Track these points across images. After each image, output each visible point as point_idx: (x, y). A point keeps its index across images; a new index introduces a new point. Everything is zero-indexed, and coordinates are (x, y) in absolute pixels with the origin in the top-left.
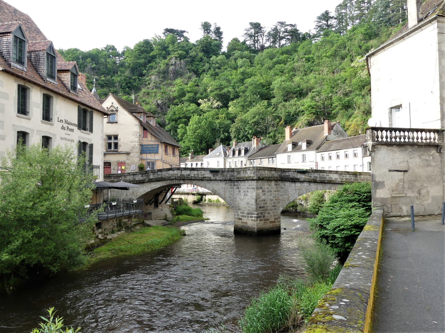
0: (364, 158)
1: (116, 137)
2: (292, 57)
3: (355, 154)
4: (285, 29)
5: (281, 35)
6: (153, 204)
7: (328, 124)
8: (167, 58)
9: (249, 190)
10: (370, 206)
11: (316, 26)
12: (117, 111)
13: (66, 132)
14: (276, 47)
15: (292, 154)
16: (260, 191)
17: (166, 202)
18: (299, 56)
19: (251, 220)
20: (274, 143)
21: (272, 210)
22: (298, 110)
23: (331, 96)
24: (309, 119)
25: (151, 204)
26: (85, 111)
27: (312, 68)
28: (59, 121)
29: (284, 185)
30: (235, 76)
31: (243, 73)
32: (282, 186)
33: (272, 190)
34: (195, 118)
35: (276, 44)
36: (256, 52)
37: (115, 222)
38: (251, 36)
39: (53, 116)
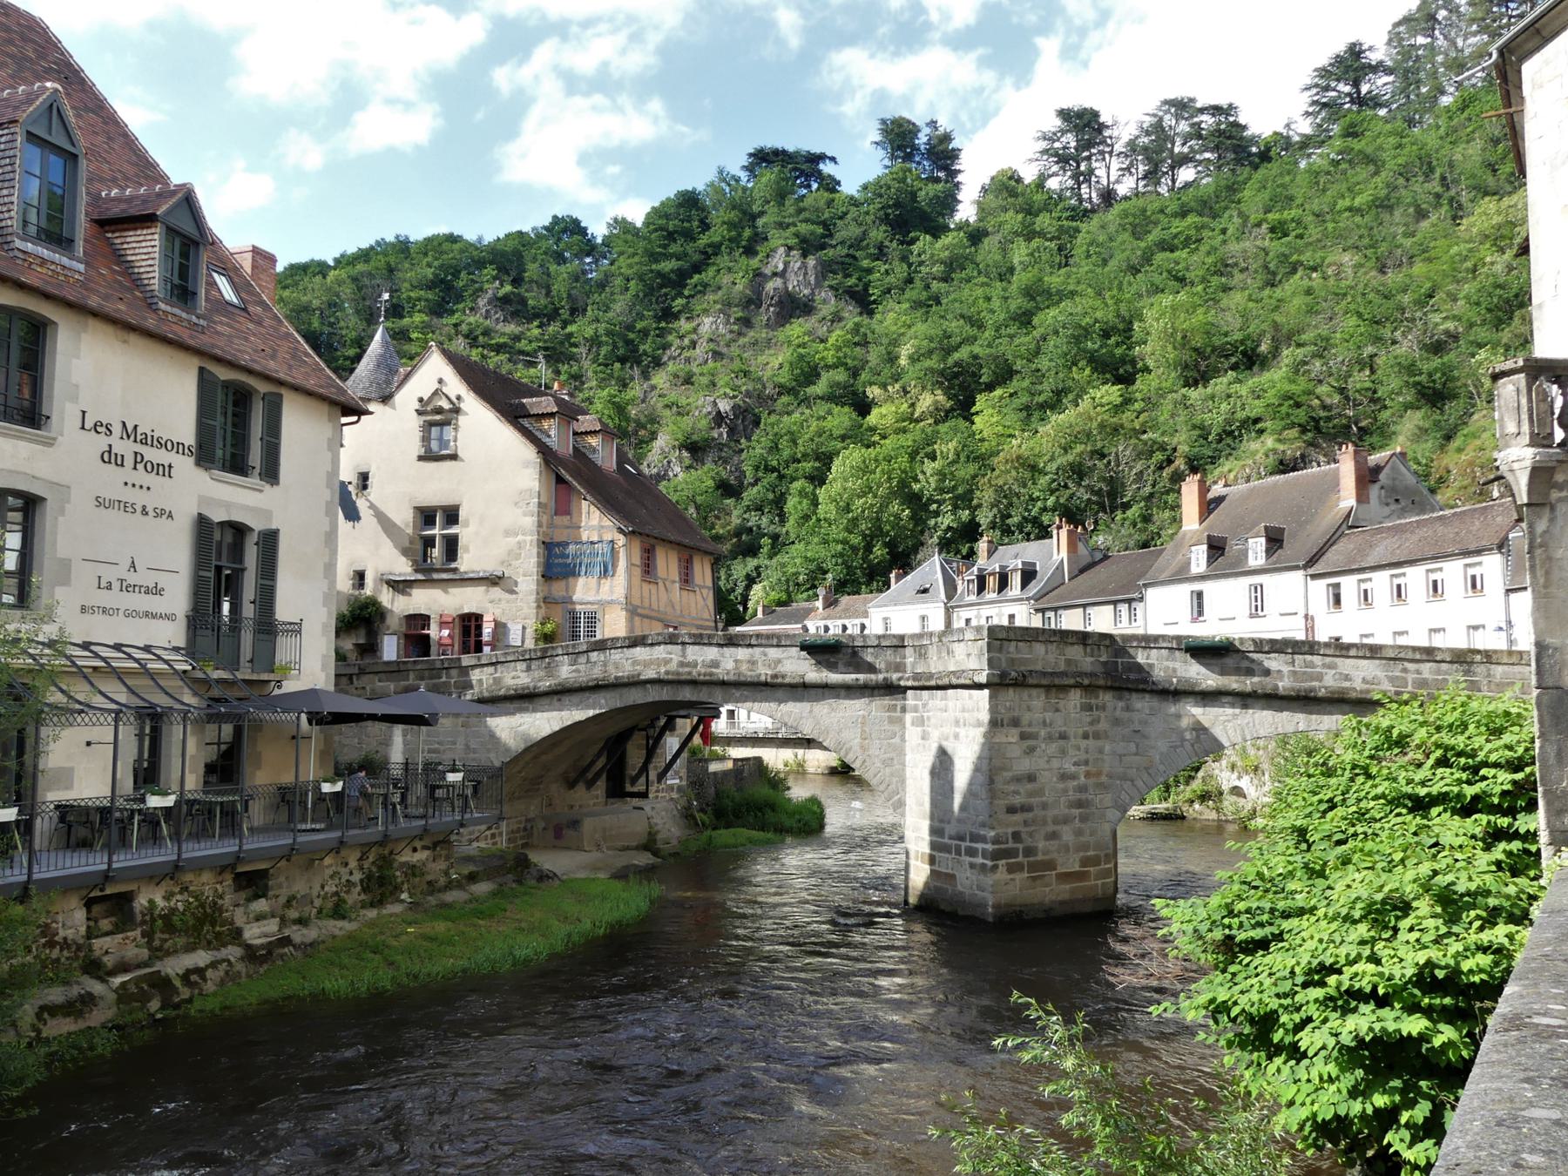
0: (1513, 596)
1: (452, 515)
2: (1218, 225)
3: (1474, 578)
4: (1192, 125)
5: (1177, 150)
6: (601, 784)
7: (1357, 462)
8: (756, 253)
9: (962, 731)
10: (1531, 836)
11: (1314, 103)
12: (457, 411)
13: (127, 473)
14: (1159, 194)
15: (1208, 587)
16: (1012, 736)
17: (662, 776)
18: (1244, 217)
19: (972, 866)
20: (1145, 545)
21: (1066, 820)
22: (1240, 415)
23: (1372, 357)
24: (1281, 447)
25: (590, 784)
26: (240, 398)
27: (1295, 257)
28: (89, 425)
29: (1128, 709)
30: (998, 303)
31: (1029, 293)
32: (1118, 713)
33: (1071, 732)
34: (847, 461)
35: (1158, 183)
36: (1081, 214)
37: (353, 864)
38: (1063, 159)
39: (55, 403)
